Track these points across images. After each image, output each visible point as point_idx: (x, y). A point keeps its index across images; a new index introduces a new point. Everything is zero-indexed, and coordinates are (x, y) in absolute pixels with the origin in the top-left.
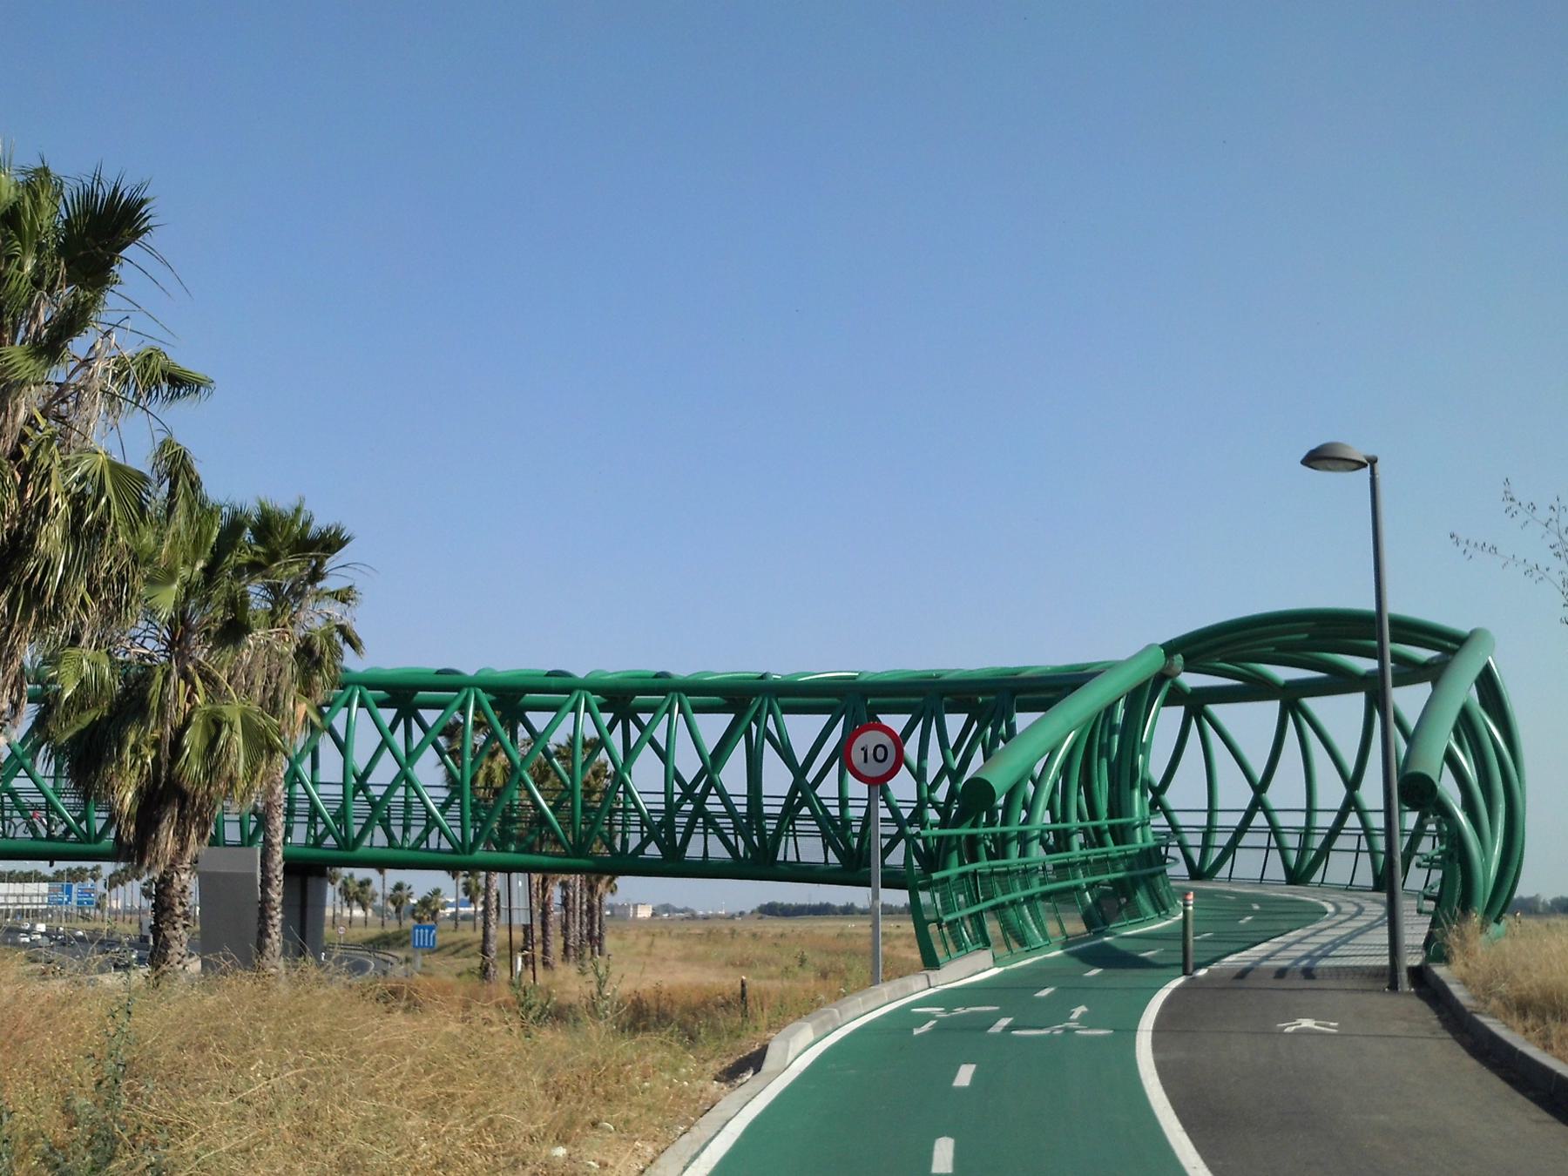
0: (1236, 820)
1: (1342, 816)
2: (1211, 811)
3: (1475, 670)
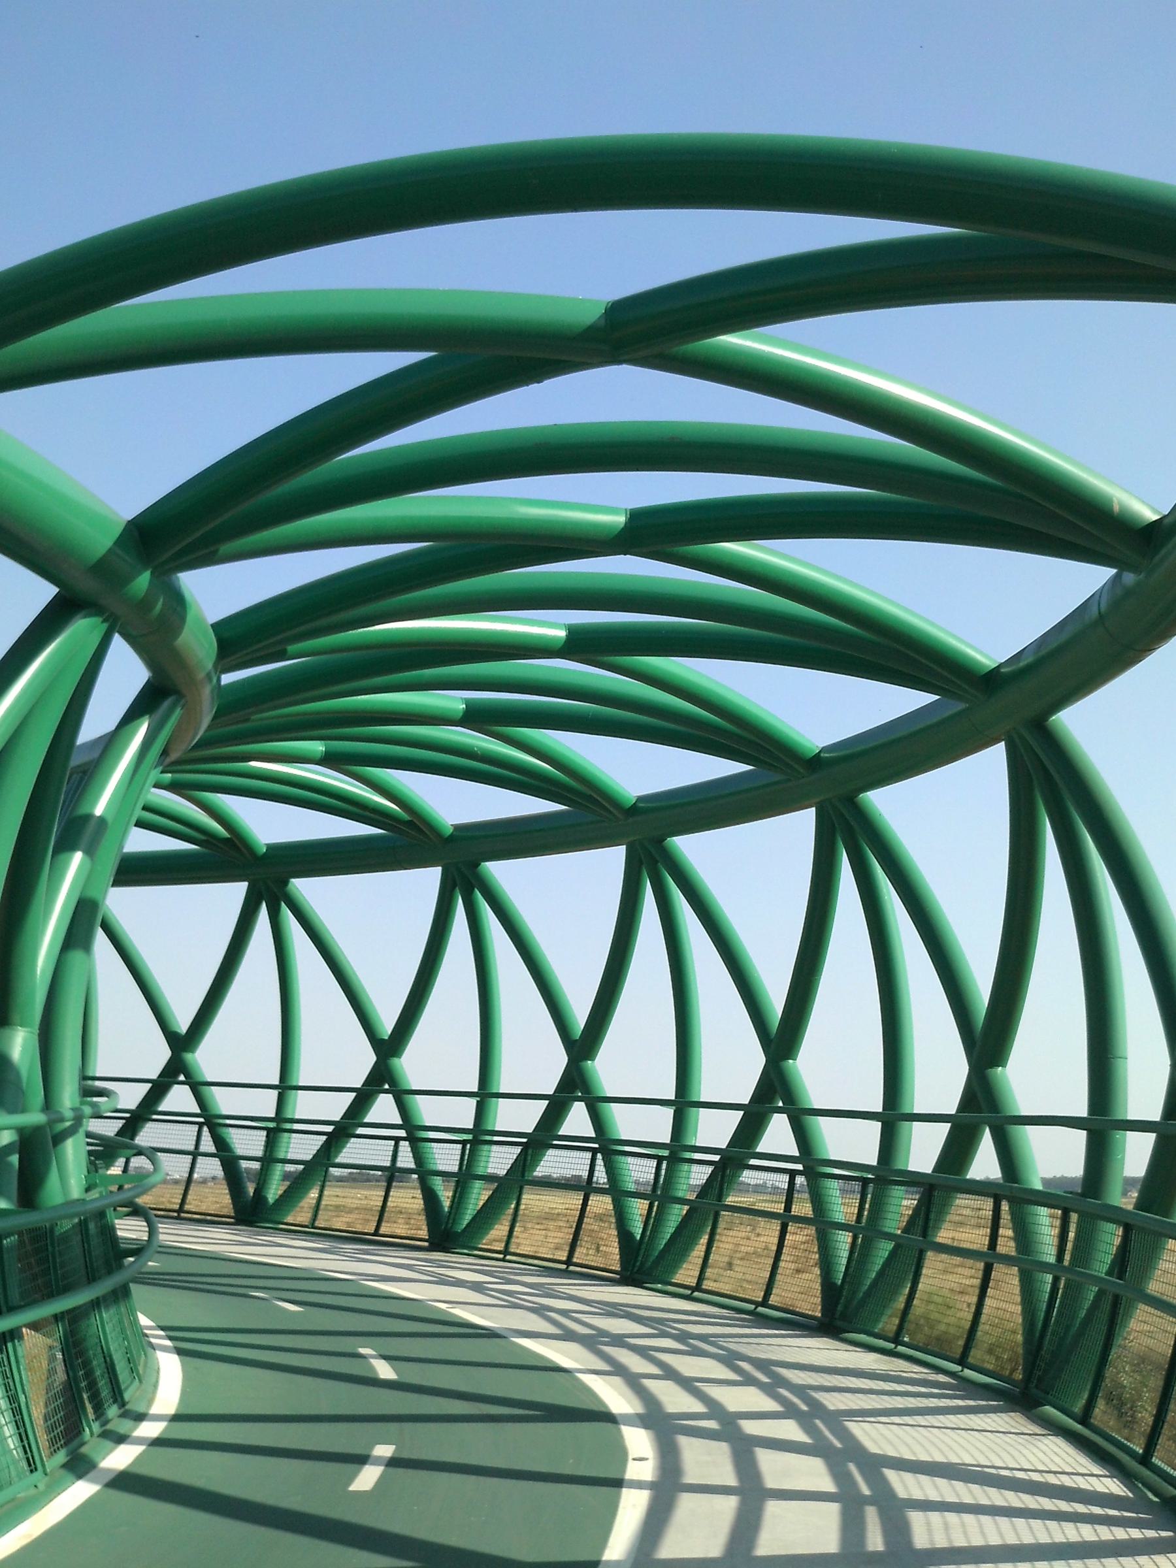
0: (335, 1107)
1: (753, 1121)
2: (285, 1087)
3: (99, 921)
